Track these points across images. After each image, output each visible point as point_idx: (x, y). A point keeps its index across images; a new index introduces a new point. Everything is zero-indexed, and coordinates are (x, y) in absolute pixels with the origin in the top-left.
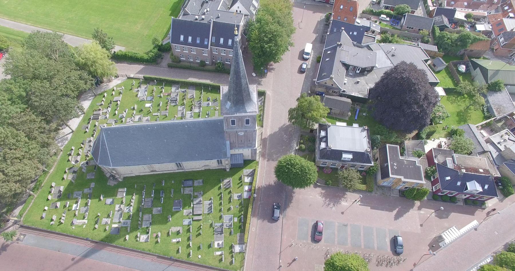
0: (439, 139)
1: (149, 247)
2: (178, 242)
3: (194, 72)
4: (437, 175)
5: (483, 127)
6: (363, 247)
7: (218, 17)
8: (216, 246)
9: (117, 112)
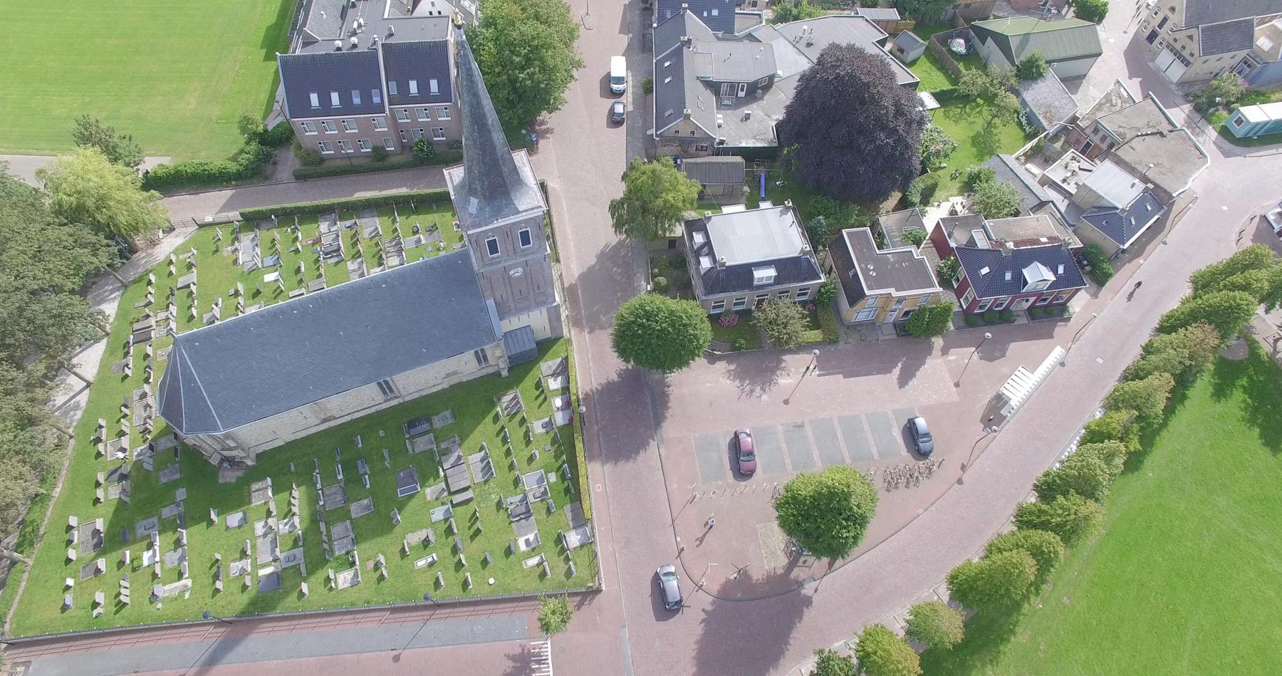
1: (367, 592)
2: (431, 565)
3: (362, 178)
4: (962, 272)
5: (1029, 157)
7: (391, 35)
8: (523, 547)
9: (194, 311)
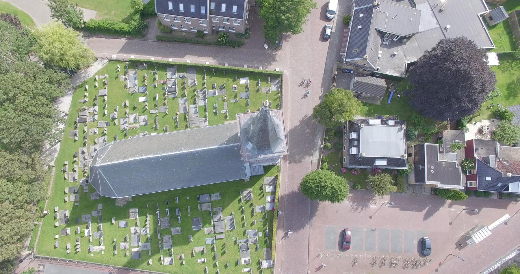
0: (480, 121)
2: (204, 262)
3: (190, 46)
6: (390, 251)
8: (243, 263)
